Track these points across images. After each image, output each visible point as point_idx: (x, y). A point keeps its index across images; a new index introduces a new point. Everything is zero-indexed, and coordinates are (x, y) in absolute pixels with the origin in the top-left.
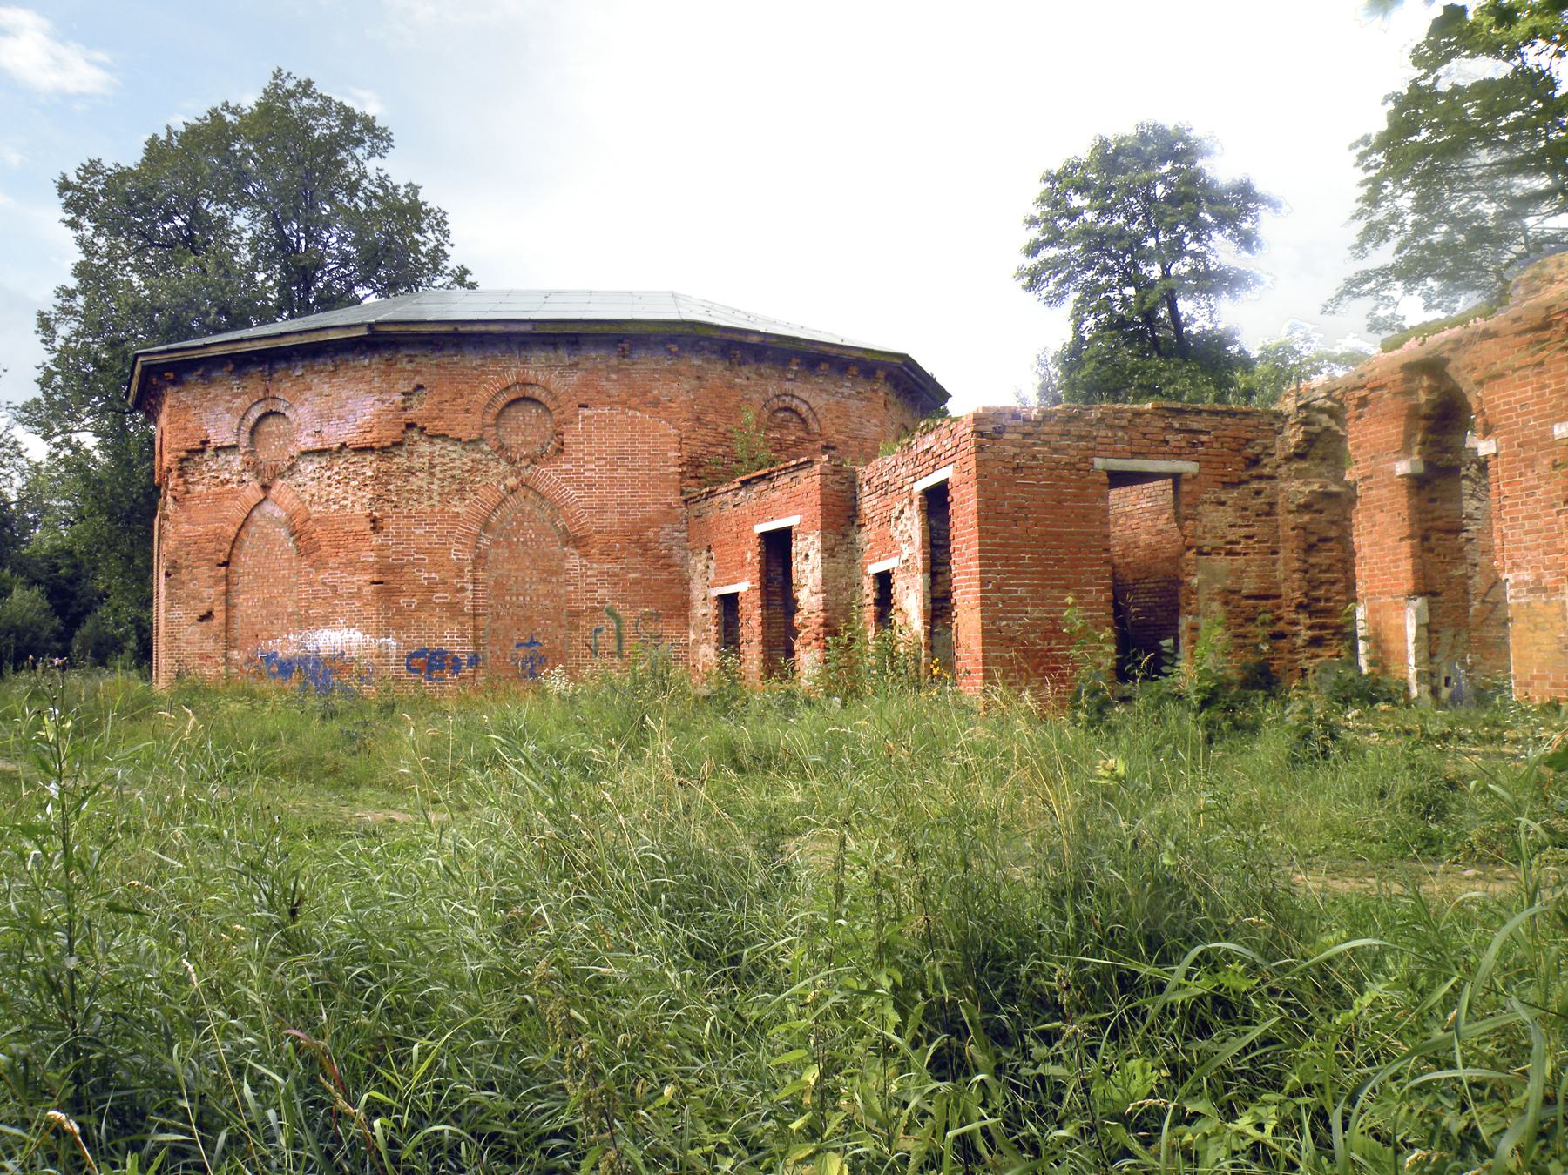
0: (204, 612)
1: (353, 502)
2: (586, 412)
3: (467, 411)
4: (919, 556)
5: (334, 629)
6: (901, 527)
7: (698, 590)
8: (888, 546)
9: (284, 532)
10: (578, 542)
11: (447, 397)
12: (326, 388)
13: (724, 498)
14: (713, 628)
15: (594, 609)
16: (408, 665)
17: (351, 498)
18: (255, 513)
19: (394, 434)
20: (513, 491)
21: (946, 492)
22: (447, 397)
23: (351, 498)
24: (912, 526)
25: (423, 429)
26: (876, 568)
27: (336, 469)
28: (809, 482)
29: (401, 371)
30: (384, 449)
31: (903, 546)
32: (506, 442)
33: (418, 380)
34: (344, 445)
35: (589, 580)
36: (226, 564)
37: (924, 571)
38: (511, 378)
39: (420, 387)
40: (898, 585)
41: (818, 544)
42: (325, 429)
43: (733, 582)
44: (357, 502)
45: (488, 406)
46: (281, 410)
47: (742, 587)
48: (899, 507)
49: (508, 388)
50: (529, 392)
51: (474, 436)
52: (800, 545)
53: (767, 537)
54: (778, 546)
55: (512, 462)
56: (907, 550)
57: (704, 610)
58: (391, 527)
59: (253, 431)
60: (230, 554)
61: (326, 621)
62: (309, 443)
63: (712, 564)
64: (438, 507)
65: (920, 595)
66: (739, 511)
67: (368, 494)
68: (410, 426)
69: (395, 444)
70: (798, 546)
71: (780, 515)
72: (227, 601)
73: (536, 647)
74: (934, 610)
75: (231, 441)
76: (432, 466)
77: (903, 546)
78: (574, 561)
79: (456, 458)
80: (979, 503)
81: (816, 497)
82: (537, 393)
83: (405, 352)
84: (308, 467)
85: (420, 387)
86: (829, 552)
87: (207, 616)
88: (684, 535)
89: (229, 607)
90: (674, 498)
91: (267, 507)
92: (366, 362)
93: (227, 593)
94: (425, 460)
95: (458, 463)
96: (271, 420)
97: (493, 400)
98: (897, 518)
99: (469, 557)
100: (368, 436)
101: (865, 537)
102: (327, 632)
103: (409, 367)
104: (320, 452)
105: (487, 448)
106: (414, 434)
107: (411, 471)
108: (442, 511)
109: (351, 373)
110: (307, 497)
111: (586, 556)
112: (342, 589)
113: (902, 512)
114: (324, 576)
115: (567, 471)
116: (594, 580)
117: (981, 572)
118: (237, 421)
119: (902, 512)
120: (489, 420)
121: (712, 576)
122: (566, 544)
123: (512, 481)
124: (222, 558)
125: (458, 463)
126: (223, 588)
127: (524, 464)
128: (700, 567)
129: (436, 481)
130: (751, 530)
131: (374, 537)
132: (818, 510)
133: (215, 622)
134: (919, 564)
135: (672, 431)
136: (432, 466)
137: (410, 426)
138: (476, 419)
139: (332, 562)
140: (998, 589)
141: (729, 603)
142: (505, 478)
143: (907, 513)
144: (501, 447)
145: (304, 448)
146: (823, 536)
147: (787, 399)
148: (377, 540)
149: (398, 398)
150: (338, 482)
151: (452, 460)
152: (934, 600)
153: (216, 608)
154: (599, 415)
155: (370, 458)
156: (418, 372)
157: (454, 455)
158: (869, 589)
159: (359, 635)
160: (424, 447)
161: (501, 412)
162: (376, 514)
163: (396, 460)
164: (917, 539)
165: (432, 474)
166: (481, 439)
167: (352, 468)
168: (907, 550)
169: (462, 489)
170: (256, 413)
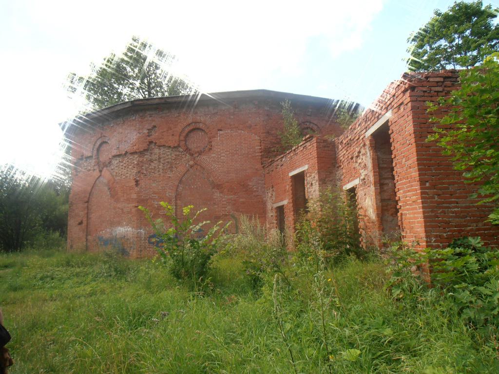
0: (80, 221)
1: (130, 175)
2: (221, 132)
3: (173, 135)
4: (371, 175)
5: (122, 226)
6: (359, 161)
7: (269, 205)
8: (355, 174)
9: (106, 188)
10: (218, 187)
11: (165, 130)
12: (121, 130)
13: (277, 163)
14: (275, 222)
15: (226, 215)
16: (149, 241)
17: (129, 173)
18: (97, 181)
19: (145, 146)
20: (191, 166)
21: (388, 137)
22: (165, 130)
23: (129, 173)
24: (367, 158)
25: (156, 143)
26: (349, 186)
27: (124, 162)
28: (312, 147)
29: (147, 121)
30: (141, 153)
31: (361, 171)
32: (189, 147)
33: (153, 124)
34: (126, 152)
35: (223, 203)
36: (87, 202)
37: (375, 183)
38: (190, 120)
39: (155, 127)
40: (360, 194)
41: (317, 177)
42: (120, 146)
43: (282, 200)
44: (131, 173)
45: (181, 132)
46: (106, 141)
47: (285, 202)
48: (357, 150)
49: (189, 124)
50: (198, 126)
51: (176, 145)
52: (308, 179)
53: (294, 177)
54: (299, 179)
55: (192, 155)
56: (363, 173)
57: (271, 214)
58: (142, 183)
59: (98, 150)
60: (89, 198)
61: (119, 224)
62: (115, 152)
63: (274, 194)
64: (162, 174)
65: (373, 197)
66: (283, 167)
67: (135, 171)
68: (151, 142)
69: (145, 150)
70: (308, 179)
71: (299, 166)
72: (87, 217)
73: (202, 232)
74: (382, 206)
75: (90, 154)
76: (160, 158)
77: (361, 171)
78: (217, 195)
79: (170, 155)
80: (414, 126)
81: (315, 154)
82: (201, 126)
83: (148, 113)
84: (115, 162)
85: (155, 127)
86: (323, 182)
87: (81, 223)
88: (263, 182)
89: (88, 218)
90: (259, 166)
91: (101, 179)
92: (134, 118)
93: (87, 213)
94: (157, 156)
95: (170, 156)
96: (104, 145)
97: (183, 130)
98: (357, 157)
99: (174, 195)
100: (135, 147)
101: (343, 171)
102: (119, 228)
103: (150, 119)
104: (119, 156)
105: (182, 150)
106: (153, 146)
107: (151, 161)
108: (164, 176)
109: (129, 123)
110: (115, 174)
111: (221, 192)
112: (125, 210)
113: (359, 152)
114: (119, 205)
115: (213, 157)
116: (225, 203)
117: (420, 175)
118: (92, 146)
119: (359, 152)
120: (182, 138)
121: (274, 198)
122: (213, 188)
123: (191, 163)
124: (86, 199)
125: (170, 156)
126: (86, 211)
127: (196, 155)
128: (270, 195)
129: (161, 164)
130: (288, 175)
131: (136, 188)
132: (315, 160)
133: (83, 225)
134: (372, 179)
135: (257, 138)
136: (160, 158)
137: (151, 142)
138: (177, 138)
139: (122, 199)
140: (433, 186)
141: (281, 209)
142: (189, 162)
143: (363, 151)
144: (187, 149)
145: (113, 154)
146: (319, 173)
147: (308, 124)
148: (137, 189)
149: (146, 131)
150: (125, 167)
151: (168, 155)
152: (382, 200)
153: (84, 219)
154: (226, 133)
155: (136, 156)
156: (153, 121)
157: (168, 153)
158: (344, 197)
159: (130, 229)
160: (157, 151)
161: (187, 135)
162: (138, 179)
163: (146, 156)
164: (370, 165)
165: (160, 162)
166: (179, 146)
167: (130, 161)
168: (363, 173)
169: (171, 167)
170: (98, 143)
